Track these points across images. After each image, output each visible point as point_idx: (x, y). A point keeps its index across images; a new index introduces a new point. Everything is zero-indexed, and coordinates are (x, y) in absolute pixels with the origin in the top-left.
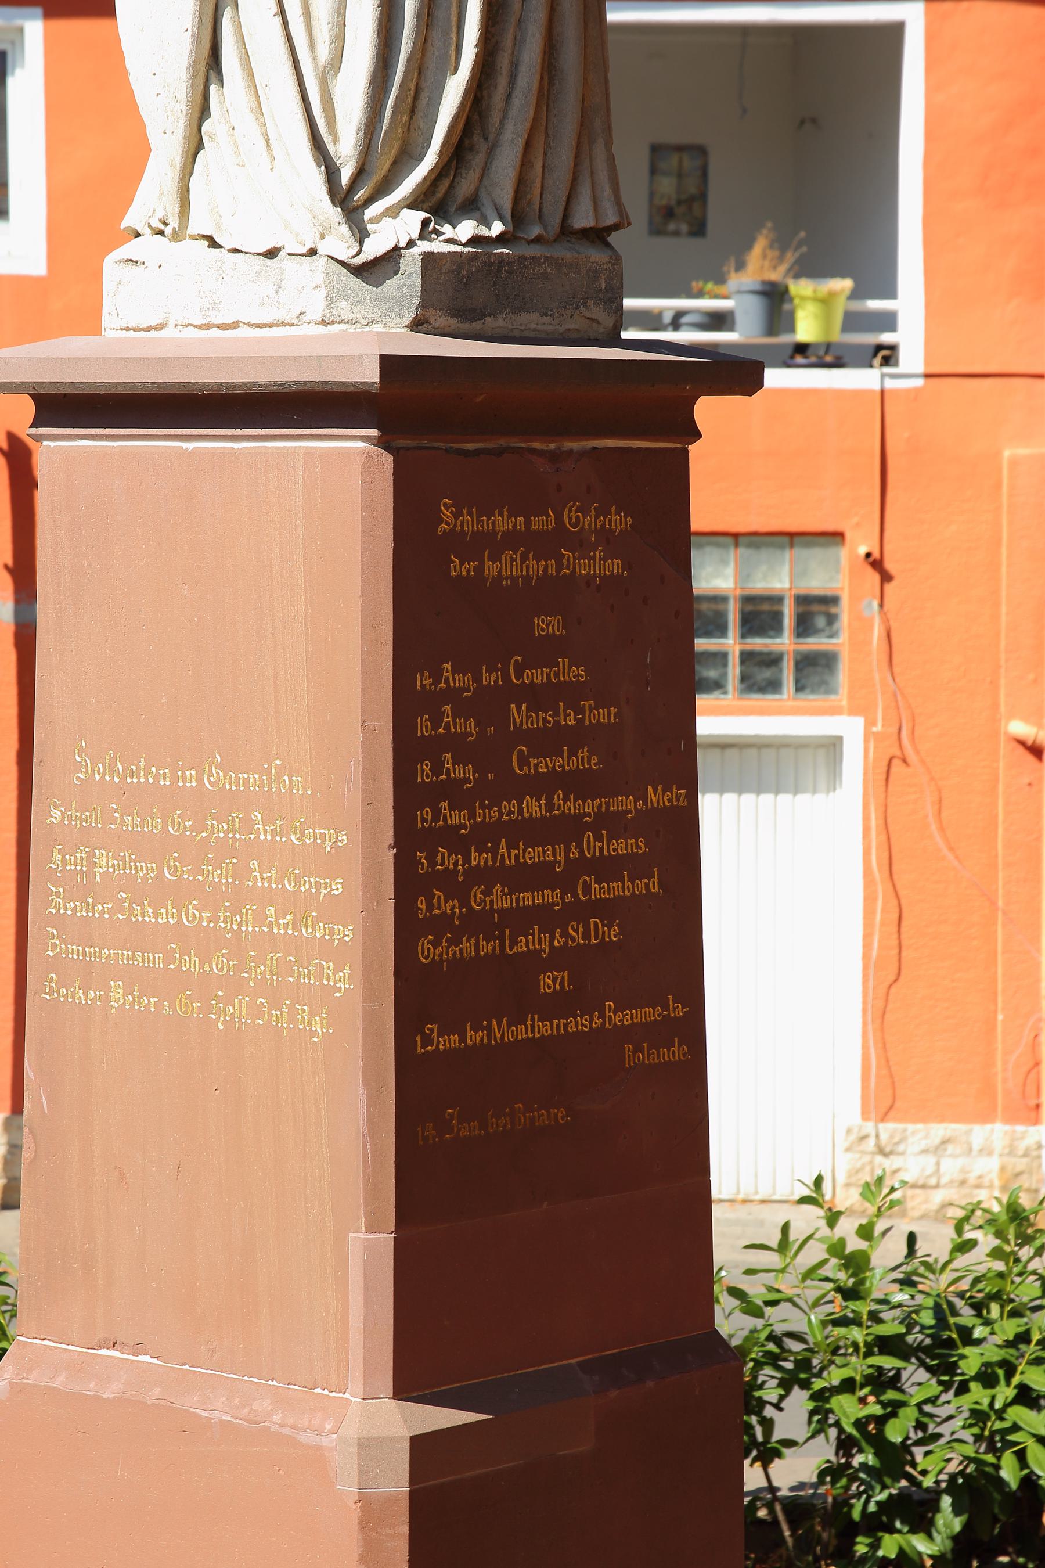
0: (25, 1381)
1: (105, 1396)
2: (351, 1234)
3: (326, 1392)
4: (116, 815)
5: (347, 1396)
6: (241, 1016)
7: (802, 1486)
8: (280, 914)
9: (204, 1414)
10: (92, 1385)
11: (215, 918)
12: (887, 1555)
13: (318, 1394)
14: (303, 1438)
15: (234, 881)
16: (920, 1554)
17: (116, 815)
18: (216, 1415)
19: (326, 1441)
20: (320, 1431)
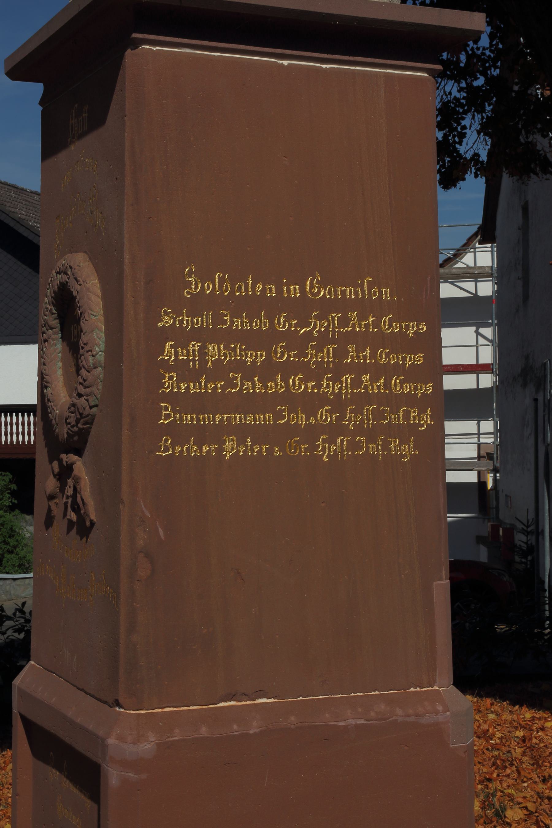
0: (171, 739)
1: (251, 732)
2: (435, 583)
3: (418, 689)
4: (226, 318)
5: (435, 688)
6: (342, 451)
7: (439, 171)
8: (374, 379)
9: (341, 724)
10: (235, 727)
11: (319, 386)
12: (60, 359)
13: (413, 692)
14: (424, 720)
15: (334, 359)
16: (88, 515)
17: (226, 318)
18: (352, 722)
19: (441, 718)
20: (437, 713)
